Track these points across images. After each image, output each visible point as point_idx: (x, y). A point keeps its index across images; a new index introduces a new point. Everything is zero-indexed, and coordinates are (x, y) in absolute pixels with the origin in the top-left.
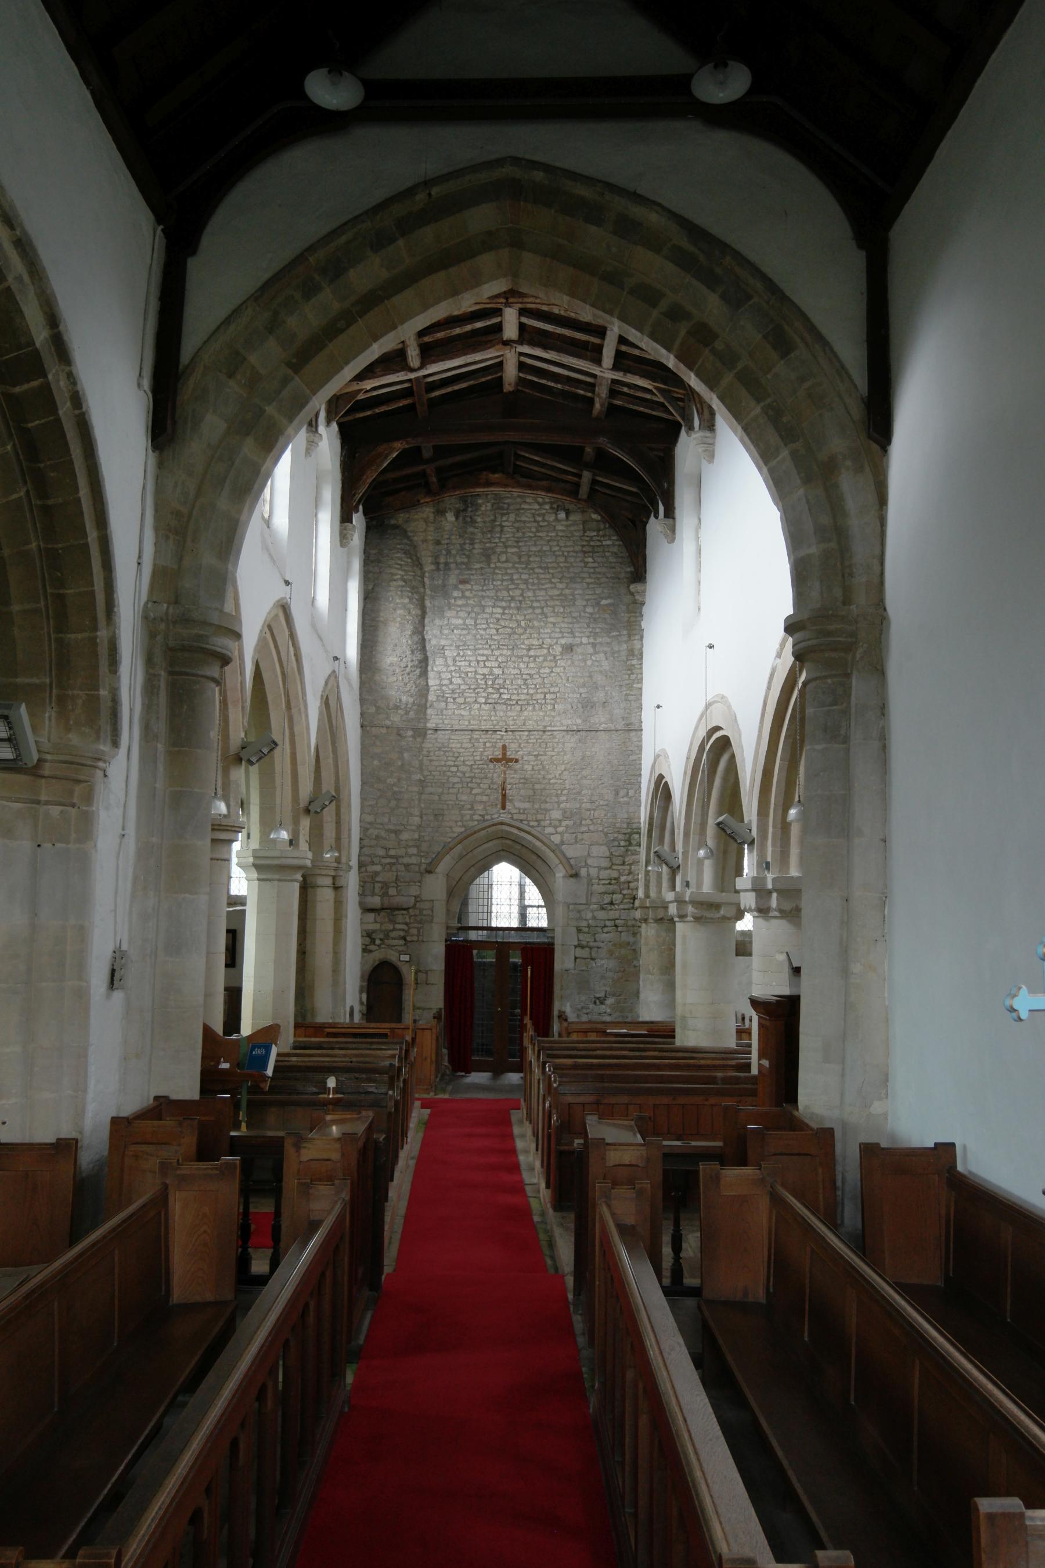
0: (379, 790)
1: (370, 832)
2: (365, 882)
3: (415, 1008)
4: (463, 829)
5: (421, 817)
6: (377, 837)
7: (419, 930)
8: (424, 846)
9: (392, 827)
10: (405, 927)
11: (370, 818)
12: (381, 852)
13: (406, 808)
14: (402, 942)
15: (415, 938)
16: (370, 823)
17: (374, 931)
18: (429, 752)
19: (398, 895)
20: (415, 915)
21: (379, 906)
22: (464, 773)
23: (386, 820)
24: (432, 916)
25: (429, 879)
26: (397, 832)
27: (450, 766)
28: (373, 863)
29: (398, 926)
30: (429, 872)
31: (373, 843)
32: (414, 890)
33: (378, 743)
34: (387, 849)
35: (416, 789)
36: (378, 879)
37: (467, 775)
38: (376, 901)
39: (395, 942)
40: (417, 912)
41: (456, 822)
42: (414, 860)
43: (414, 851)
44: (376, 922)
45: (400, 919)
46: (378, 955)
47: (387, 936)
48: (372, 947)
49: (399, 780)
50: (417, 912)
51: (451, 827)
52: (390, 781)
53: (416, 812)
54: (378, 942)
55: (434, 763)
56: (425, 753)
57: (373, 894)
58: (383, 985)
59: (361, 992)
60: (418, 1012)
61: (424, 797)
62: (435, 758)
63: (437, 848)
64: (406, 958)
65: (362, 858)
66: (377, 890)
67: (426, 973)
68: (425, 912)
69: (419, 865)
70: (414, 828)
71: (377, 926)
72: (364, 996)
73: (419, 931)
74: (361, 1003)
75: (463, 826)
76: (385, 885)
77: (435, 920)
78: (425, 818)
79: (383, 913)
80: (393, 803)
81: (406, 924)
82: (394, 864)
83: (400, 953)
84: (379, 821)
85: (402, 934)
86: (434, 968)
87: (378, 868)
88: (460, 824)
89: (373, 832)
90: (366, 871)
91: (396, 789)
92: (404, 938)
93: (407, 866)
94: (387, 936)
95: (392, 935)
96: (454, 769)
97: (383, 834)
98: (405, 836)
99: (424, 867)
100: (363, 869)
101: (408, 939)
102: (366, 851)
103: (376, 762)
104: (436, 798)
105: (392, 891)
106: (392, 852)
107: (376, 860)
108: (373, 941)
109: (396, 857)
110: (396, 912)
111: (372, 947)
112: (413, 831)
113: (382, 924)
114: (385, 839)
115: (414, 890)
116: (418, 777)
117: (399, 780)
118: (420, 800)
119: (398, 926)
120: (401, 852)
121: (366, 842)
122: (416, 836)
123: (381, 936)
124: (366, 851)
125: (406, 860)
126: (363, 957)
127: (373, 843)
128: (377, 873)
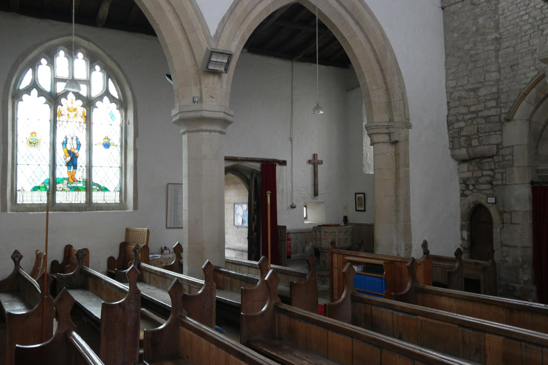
0: (452, 73)
1: (453, 95)
2: (453, 138)
3: (503, 245)
4: (536, 73)
5: (499, 72)
6: (460, 98)
7: (502, 174)
8: (503, 98)
9: (470, 87)
10: (491, 173)
11: (453, 83)
12: (463, 110)
13: (483, 67)
14: (489, 186)
15: (500, 182)
16: (453, 88)
17: (468, 179)
18: (503, 10)
19: (480, 145)
20: (499, 162)
21: (466, 157)
22: (535, 18)
23: (465, 82)
24: (513, 160)
25: (509, 126)
26: (475, 90)
27: (522, 16)
28: (458, 121)
29: (485, 173)
30: (508, 120)
31: (457, 103)
32: (495, 139)
33: (456, 18)
34: (469, 107)
35: (492, 47)
36: (463, 133)
37: (538, 18)
38: (463, 152)
39: (483, 187)
40: (501, 158)
41: (529, 67)
42: (493, 112)
43: (493, 103)
44: (469, 171)
45: (486, 166)
46: (471, 199)
47: (477, 182)
48: (467, 192)
49: (475, 44)
50: (501, 158)
51: (525, 74)
52: (467, 47)
53: (493, 68)
54: (471, 187)
55: (509, 18)
56: (500, 12)
57: (461, 147)
58: (478, 221)
59: (462, 229)
60: (505, 249)
61: (501, 53)
62: (509, 14)
63: (514, 97)
64: (492, 200)
65: (450, 118)
66: (463, 144)
67: (510, 213)
68: (506, 158)
69: (500, 116)
70: (492, 83)
71: (469, 174)
72: (465, 234)
73: (502, 176)
74: (463, 239)
75: (536, 69)
76: (469, 138)
77: (516, 164)
78: (502, 71)
79: (473, 163)
80: (471, 65)
81: (492, 170)
82: (475, 118)
83: (488, 196)
84: (460, 84)
85: (488, 179)
86: (517, 209)
87: (462, 124)
88: (533, 68)
89: (456, 94)
90: (453, 128)
91: (472, 52)
92: (491, 183)
93: (486, 118)
94: (477, 182)
95: (481, 180)
96: (526, 17)
97: (463, 94)
98: (483, 92)
99: (503, 116)
100: (451, 127)
101: (494, 183)
102: (452, 111)
103: (455, 35)
104: (511, 50)
105: (475, 143)
106: (473, 109)
107: (460, 118)
108: (467, 186)
109: (476, 112)
110: (484, 161)
111: (467, 192)
112: (492, 86)
113: (473, 172)
114: (465, 98)
115: (495, 139)
116: (494, 35)
117: (475, 44)
118: (497, 57)
119: (485, 173)
120: (481, 107)
121: (452, 105)
122: (494, 90)
123: (473, 182)
124: (452, 111)
125: (486, 113)
126: (461, 200)
127: (457, 103)
128: (461, 129)
